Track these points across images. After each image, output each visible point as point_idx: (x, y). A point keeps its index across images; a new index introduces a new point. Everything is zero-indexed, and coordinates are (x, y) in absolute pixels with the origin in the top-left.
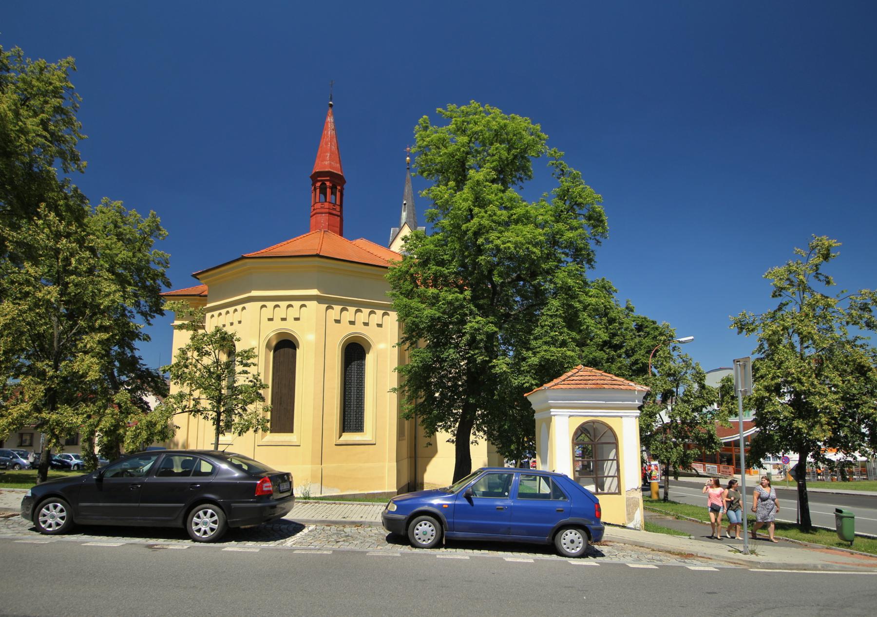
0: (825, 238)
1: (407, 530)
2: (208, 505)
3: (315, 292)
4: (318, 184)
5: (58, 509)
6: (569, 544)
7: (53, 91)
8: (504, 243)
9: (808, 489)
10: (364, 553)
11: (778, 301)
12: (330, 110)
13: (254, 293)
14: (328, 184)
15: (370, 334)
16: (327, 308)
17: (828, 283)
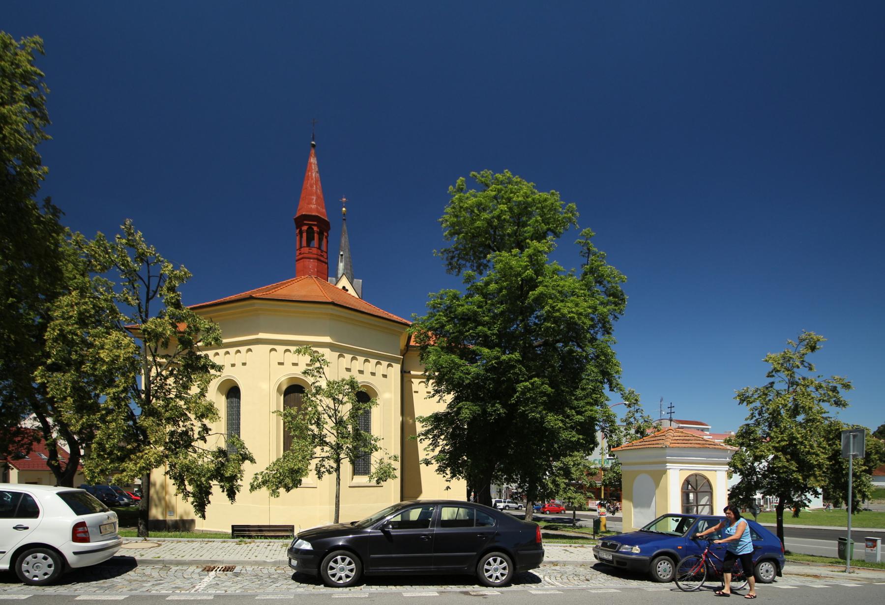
0: (812, 333)
1: (319, 568)
2: (497, 553)
3: (327, 339)
4: (305, 228)
5: (339, 560)
6: (765, 573)
7: (21, 75)
8: (569, 312)
9: (784, 525)
10: (164, 596)
11: (771, 380)
12: (313, 151)
13: (262, 336)
14: (315, 228)
15: (376, 383)
16: (340, 356)
17: (811, 369)
